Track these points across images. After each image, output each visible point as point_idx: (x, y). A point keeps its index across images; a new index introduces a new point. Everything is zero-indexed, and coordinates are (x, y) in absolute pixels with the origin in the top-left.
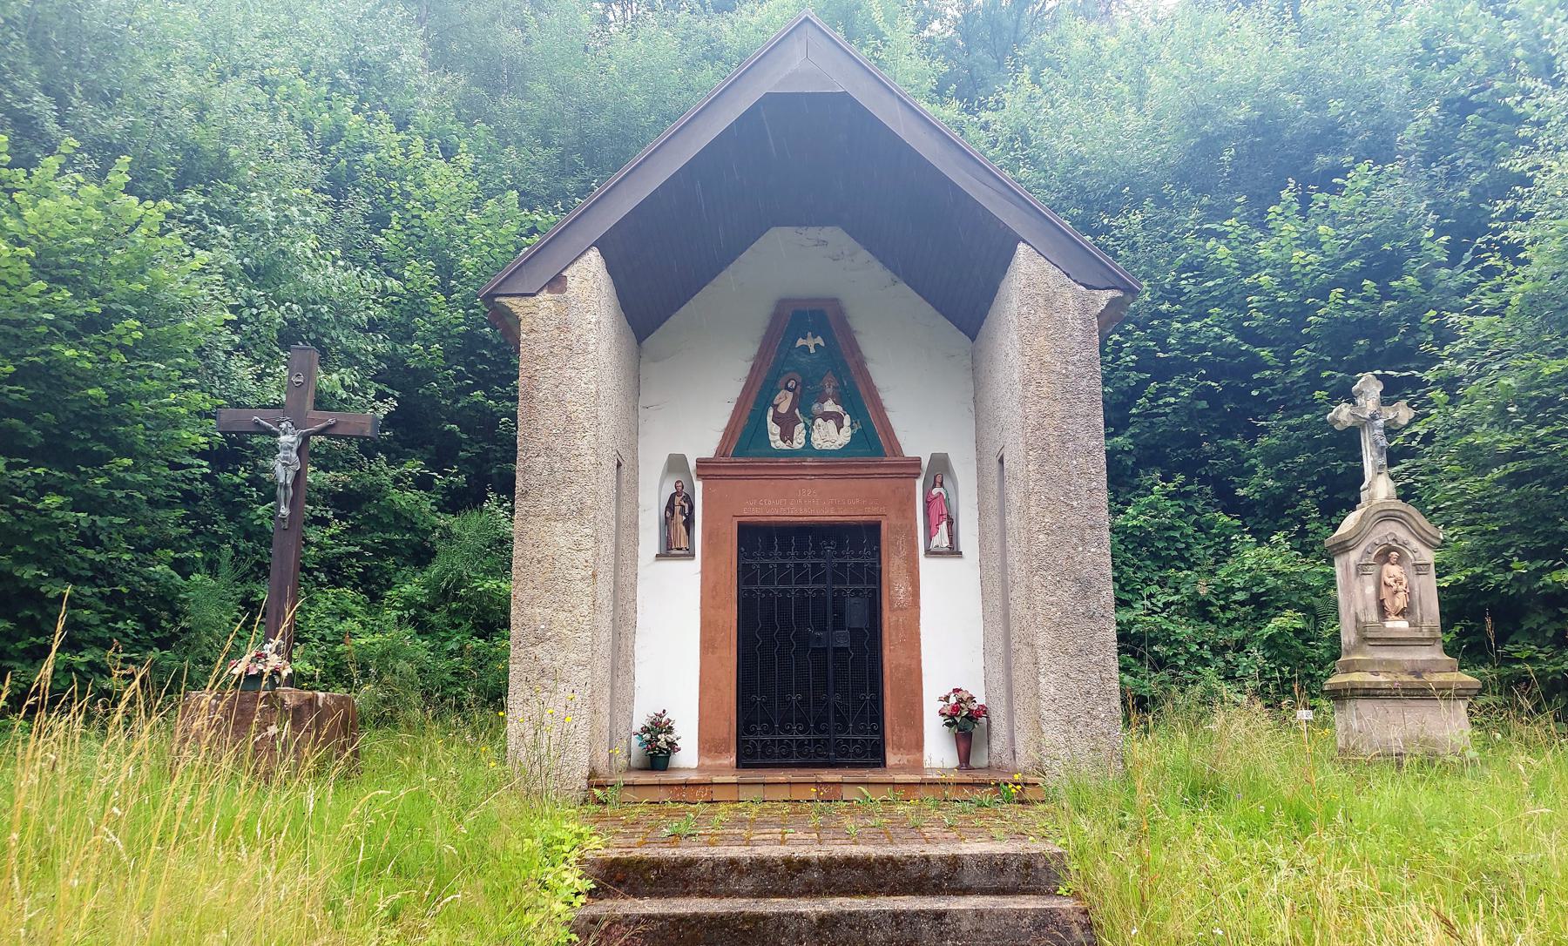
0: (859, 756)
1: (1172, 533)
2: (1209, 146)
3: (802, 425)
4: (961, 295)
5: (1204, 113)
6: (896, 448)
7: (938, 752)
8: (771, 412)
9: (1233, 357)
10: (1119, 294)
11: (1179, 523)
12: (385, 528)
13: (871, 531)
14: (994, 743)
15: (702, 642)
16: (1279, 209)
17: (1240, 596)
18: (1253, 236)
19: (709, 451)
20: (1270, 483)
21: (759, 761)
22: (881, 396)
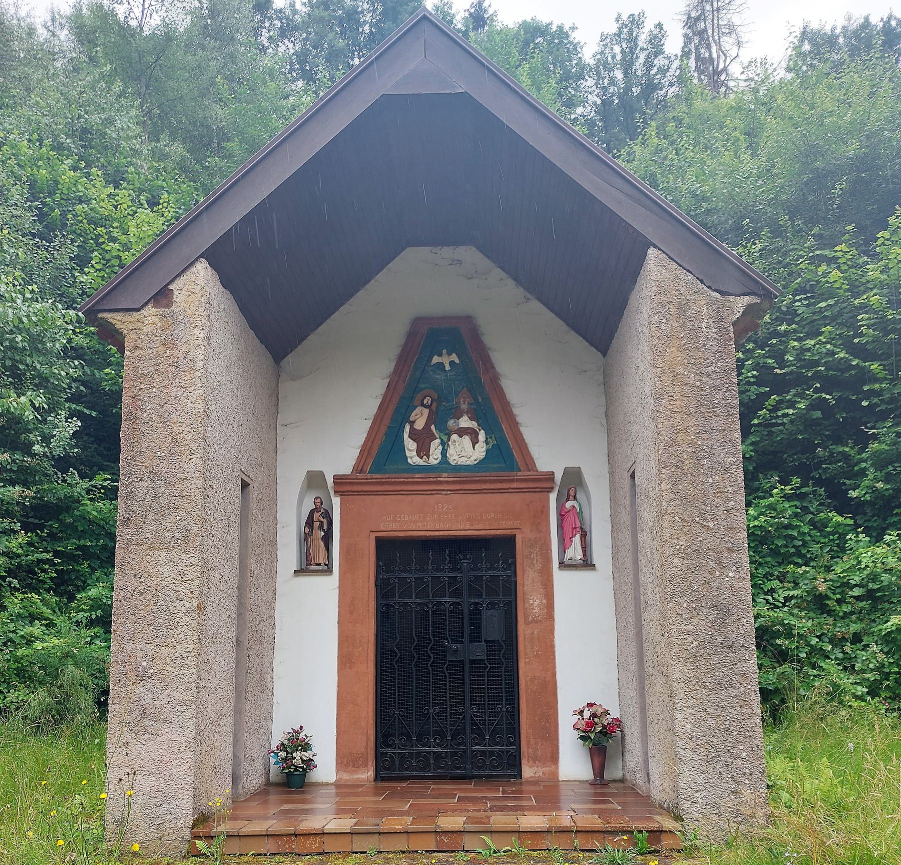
0: (495, 767)
1: (790, 532)
2: (820, 181)
3: (438, 441)
4: (594, 319)
5: (814, 151)
6: (530, 463)
7: (573, 763)
8: (407, 428)
9: (842, 371)
10: (755, 300)
11: (796, 522)
12: (82, 535)
13: (507, 544)
14: (628, 757)
15: (341, 657)
16: (887, 234)
17: (857, 592)
18: (861, 260)
19: (346, 466)
20: (880, 485)
21: (396, 774)
22: (516, 411)
